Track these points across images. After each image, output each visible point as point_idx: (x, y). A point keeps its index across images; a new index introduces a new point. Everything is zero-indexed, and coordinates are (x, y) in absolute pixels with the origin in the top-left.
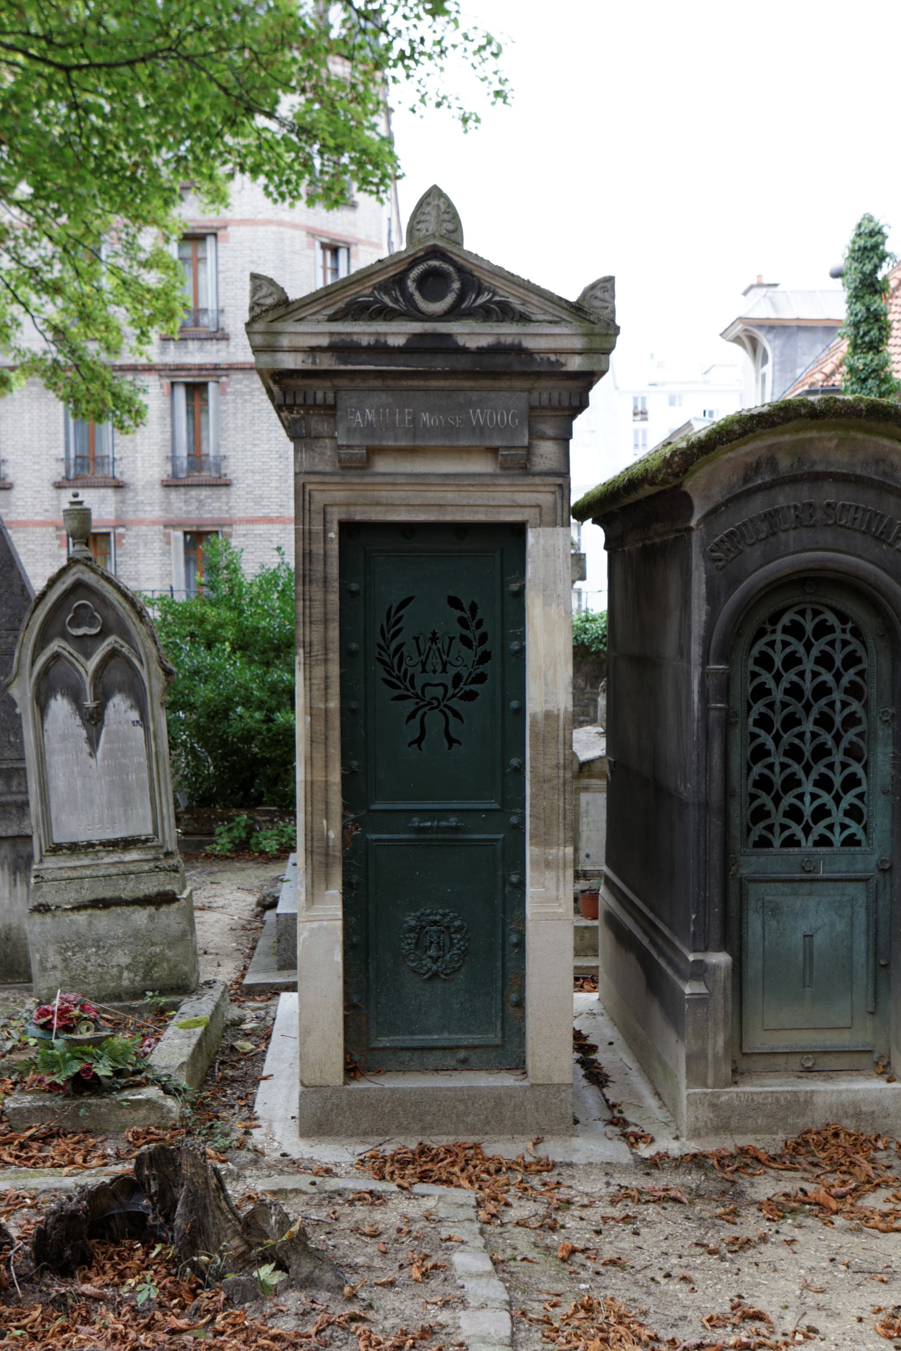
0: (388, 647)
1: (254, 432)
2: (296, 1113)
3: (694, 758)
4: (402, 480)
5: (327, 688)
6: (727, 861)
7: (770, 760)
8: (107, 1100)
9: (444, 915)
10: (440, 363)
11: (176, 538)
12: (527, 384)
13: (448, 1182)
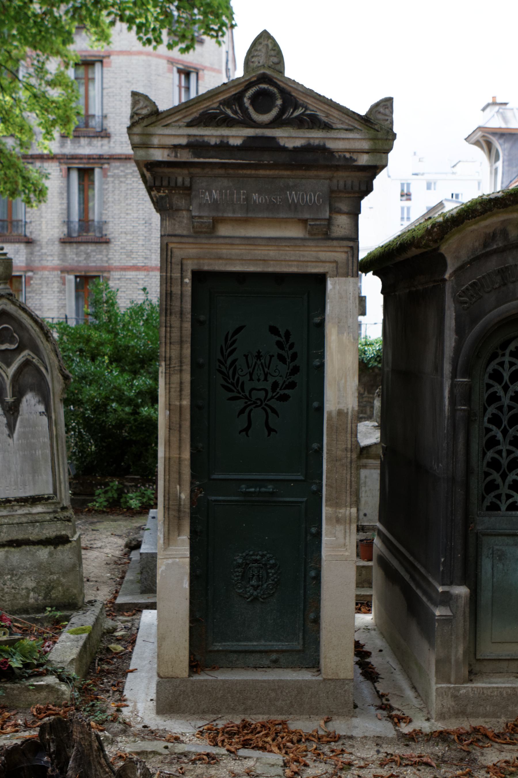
0: (226, 362)
1: (127, 205)
2: (154, 696)
3: (445, 445)
4: (237, 241)
5: (181, 390)
6: (468, 519)
7: (500, 447)
8: (18, 685)
9: (263, 556)
10: (267, 158)
11: (70, 280)
12: (328, 174)
13: (263, 748)
